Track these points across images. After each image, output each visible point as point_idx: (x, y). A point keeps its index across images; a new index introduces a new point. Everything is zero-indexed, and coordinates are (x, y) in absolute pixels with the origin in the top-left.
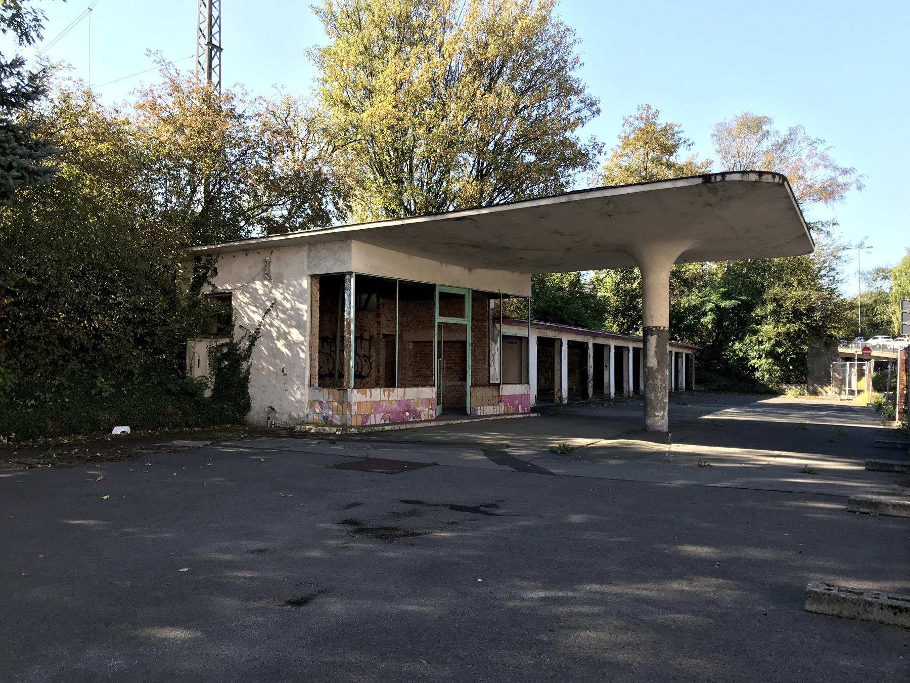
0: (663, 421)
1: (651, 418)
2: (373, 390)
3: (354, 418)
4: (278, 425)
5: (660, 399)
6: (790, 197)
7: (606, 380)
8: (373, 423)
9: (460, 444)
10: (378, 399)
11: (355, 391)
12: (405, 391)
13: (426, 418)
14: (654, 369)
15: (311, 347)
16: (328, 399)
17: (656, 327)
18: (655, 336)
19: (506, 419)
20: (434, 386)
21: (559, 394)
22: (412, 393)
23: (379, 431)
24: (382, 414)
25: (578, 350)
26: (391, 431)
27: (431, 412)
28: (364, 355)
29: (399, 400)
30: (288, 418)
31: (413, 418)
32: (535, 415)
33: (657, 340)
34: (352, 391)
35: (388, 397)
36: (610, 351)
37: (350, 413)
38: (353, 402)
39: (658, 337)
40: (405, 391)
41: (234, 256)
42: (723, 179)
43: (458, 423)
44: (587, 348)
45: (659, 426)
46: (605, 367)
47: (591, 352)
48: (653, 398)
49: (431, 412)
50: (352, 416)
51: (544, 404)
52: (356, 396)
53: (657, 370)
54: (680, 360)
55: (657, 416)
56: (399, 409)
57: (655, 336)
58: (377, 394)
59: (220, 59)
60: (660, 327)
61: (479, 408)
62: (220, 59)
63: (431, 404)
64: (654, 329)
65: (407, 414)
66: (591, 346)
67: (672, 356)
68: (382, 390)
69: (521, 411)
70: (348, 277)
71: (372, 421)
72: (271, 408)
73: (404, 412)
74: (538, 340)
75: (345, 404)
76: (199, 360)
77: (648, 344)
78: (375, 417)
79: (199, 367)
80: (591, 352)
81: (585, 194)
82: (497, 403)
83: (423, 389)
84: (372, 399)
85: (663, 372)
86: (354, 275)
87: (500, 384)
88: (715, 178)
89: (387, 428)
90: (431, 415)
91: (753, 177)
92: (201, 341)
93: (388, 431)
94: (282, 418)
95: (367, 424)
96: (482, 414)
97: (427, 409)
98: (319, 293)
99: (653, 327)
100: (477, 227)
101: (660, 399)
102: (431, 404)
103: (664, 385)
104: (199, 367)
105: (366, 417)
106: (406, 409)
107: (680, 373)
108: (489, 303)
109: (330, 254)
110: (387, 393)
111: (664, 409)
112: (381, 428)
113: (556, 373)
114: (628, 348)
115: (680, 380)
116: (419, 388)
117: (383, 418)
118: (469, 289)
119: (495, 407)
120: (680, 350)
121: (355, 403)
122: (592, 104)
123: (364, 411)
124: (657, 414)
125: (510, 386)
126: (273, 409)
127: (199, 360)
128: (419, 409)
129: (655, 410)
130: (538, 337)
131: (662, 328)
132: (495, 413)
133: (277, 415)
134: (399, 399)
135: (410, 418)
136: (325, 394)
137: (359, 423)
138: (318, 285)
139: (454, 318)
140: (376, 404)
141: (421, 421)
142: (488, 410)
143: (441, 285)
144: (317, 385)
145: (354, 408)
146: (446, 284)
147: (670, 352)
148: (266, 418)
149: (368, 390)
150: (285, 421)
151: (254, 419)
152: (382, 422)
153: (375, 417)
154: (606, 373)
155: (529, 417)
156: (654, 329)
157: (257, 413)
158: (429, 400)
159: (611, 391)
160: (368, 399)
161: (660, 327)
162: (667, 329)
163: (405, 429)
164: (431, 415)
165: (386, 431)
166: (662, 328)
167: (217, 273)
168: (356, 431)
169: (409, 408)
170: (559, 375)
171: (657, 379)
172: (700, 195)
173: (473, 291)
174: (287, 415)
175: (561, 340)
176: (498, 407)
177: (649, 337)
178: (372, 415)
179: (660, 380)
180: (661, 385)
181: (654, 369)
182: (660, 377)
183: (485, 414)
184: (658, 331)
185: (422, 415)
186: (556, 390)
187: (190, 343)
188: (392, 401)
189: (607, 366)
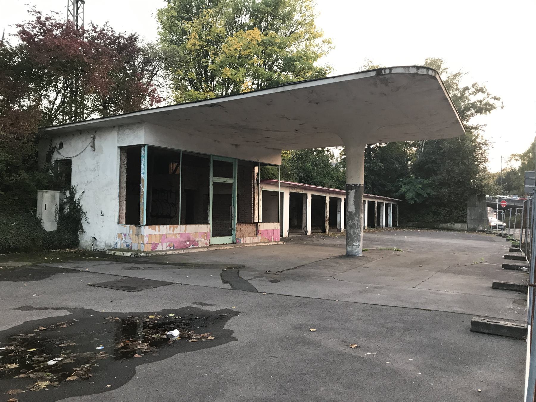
0: (359, 249)
1: (350, 247)
2: (161, 226)
3: (146, 246)
4: (98, 250)
5: (357, 234)
6: (442, 89)
7: (338, 220)
8: (161, 249)
9: (198, 266)
10: (165, 233)
11: (147, 227)
12: (186, 228)
13: (202, 245)
14: (353, 213)
15: (120, 196)
16: (130, 232)
17: (354, 184)
18: (354, 190)
19: (260, 245)
20: (209, 223)
21: (305, 228)
22: (191, 229)
23: (163, 255)
24: (168, 244)
25: (318, 202)
26: (172, 255)
27: (206, 241)
28: (172, 203)
29: (181, 234)
30: (104, 245)
31: (192, 246)
32: (282, 243)
33: (355, 193)
34: (144, 227)
35: (173, 231)
36: (383, 205)
37: (143, 242)
38: (145, 234)
39: (356, 191)
40: (186, 228)
41: (73, 135)
42: (390, 71)
43: (224, 249)
44: (375, 203)
45: (356, 252)
46: (338, 212)
47: (328, 202)
48: (352, 233)
49: (206, 241)
50: (144, 244)
51: (294, 236)
52: (147, 231)
53: (355, 214)
54: (389, 208)
55: (355, 245)
56: (182, 239)
57: (354, 190)
58: (164, 229)
59: (83, 9)
60: (357, 184)
61: (242, 238)
62: (83, 9)
63: (206, 236)
64: (353, 185)
65: (188, 243)
66: (328, 198)
67: (365, 204)
68: (168, 226)
69: (273, 241)
70: (143, 148)
71: (160, 248)
72: (94, 237)
73: (186, 242)
74: (290, 194)
75: (140, 236)
76: (46, 205)
77: (349, 196)
78: (162, 245)
79: (45, 209)
80: (328, 202)
81: (295, 85)
82: (256, 235)
83: (200, 226)
84: (160, 233)
85: (359, 215)
86: (146, 147)
87: (258, 222)
88: (385, 71)
89: (168, 253)
90: (207, 244)
91: (413, 71)
92: (47, 192)
93: (169, 255)
94: (101, 245)
95: (156, 250)
96: (244, 243)
97: (203, 239)
98: (126, 159)
99: (352, 184)
100: (226, 112)
101: (357, 234)
102: (206, 236)
103: (359, 224)
104: (45, 209)
105: (156, 245)
106: (187, 239)
107: (389, 216)
108: (254, 169)
109: (131, 132)
110: (172, 228)
111: (359, 240)
112: (164, 253)
113: (304, 216)
114: (375, 202)
115: (389, 221)
116: (197, 225)
117: (169, 246)
118: (236, 159)
119: (254, 238)
120: (381, 201)
121: (147, 235)
122: (329, 42)
123: (154, 241)
124: (354, 244)
125: (265, 223)
126: (95, 239)
127: (46, 205)
128: (197, 240)
129: (353, 241)
130: (290, 192)
131: (358, 185)
132: (254, 242)
133: (98, 243)
134: (181, 232)
135: (190, 245)
136: (129, 229)
137: (150, 249)
138: (126, 154)
139: (225, 178)
140: (163, 237)
141: (199, 248)
142: (249, 240)
143: (215, 155)
144: (124, 223)
145: (146, 239)
146: (219, 155)
147: (365, 201)
148: (91, 245)
149: (157, 226)
150: (102, 247)
151: (84, 245)
152: (168, 248)
153: (162, 245)
154: (338, 215)
155: (278, 244)
156: (353, 185)
157: (85, 240)
158: (205, 233)
159: (342, 227)
160: (157, 232)
161: (357, 184)
162: (362, 185)
163: (183, 253)
164: (207, 244)
165: (168, 255)
166: (358, 185)
167: (63, 146)
168: (145, 255)
169: (189, 239)
170: (305, 217)
171: (354, 220)
172: (375, 85)
173: (239, 160)
174: (104, 243)
175: (307, 194)
176: (256, 237)
177: (350, 191)
178: (160, 244)
179: (357, 220)
180: (358, 224)
181: (353, 213)
182: (357, 218)
183: (247, 242)
184: (356, 187)
185: (199, 243)
186: (303, 226)
187: (39, 194)
188: (176, 234)
189: (339, 211)
